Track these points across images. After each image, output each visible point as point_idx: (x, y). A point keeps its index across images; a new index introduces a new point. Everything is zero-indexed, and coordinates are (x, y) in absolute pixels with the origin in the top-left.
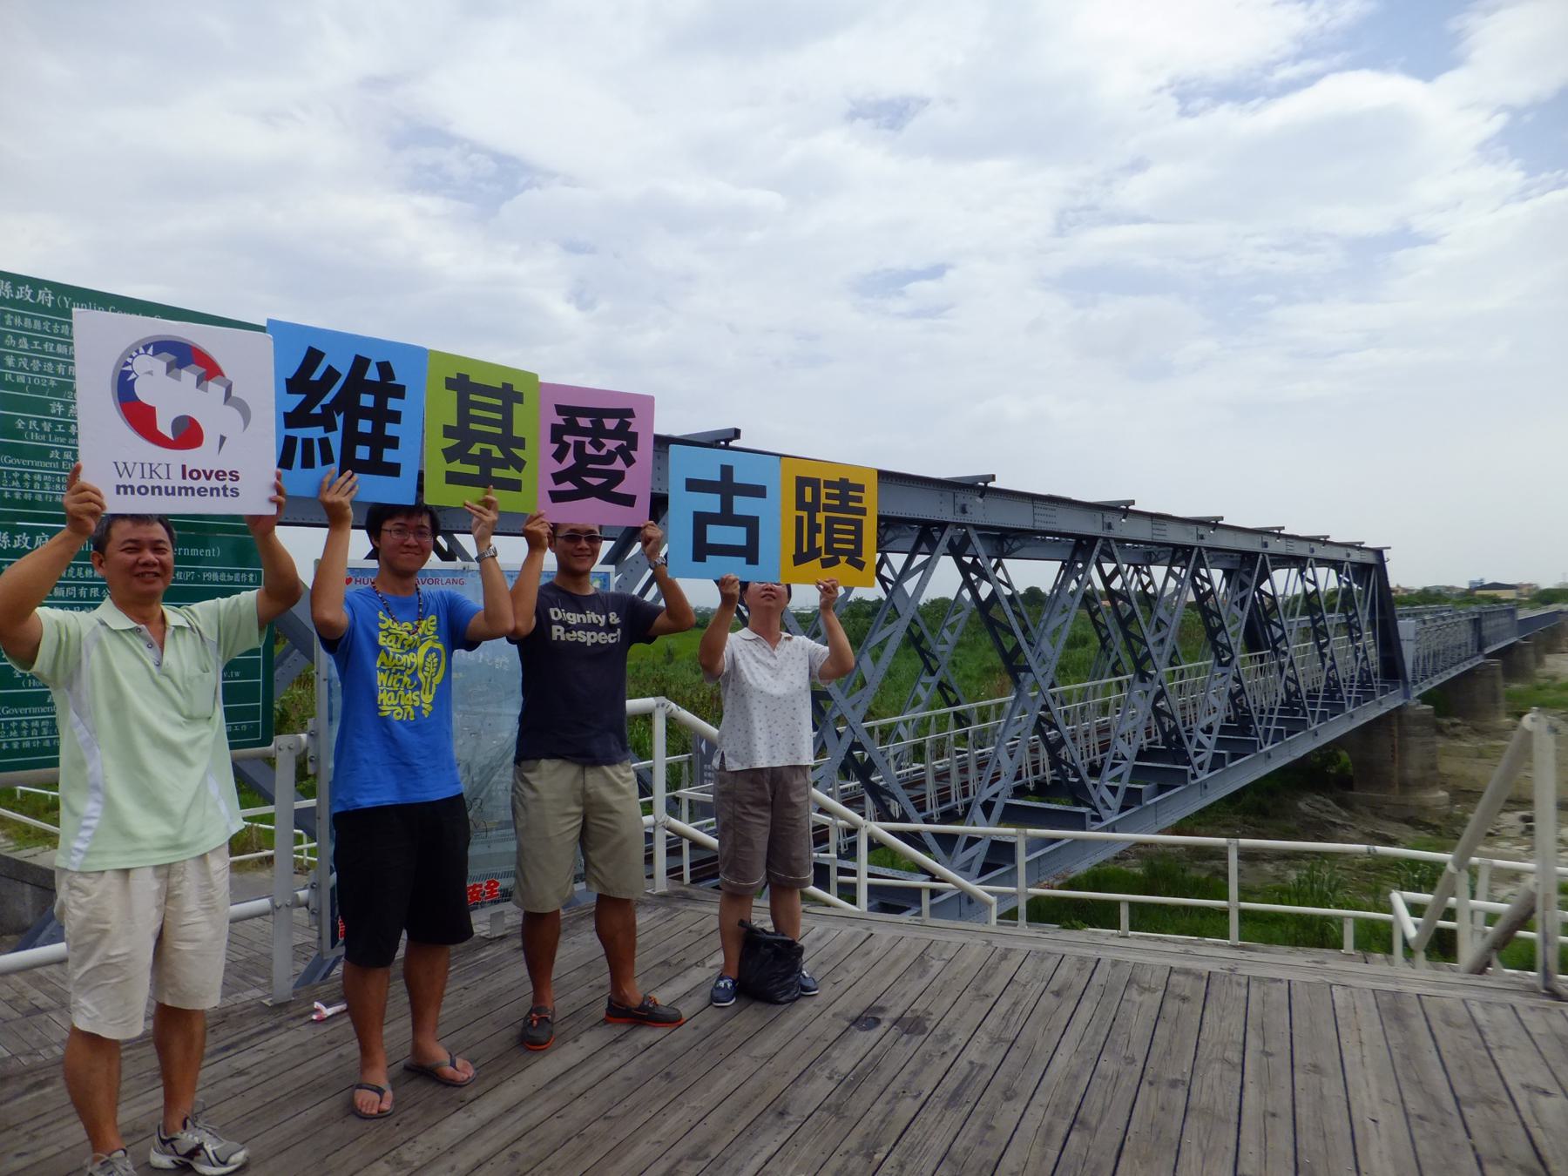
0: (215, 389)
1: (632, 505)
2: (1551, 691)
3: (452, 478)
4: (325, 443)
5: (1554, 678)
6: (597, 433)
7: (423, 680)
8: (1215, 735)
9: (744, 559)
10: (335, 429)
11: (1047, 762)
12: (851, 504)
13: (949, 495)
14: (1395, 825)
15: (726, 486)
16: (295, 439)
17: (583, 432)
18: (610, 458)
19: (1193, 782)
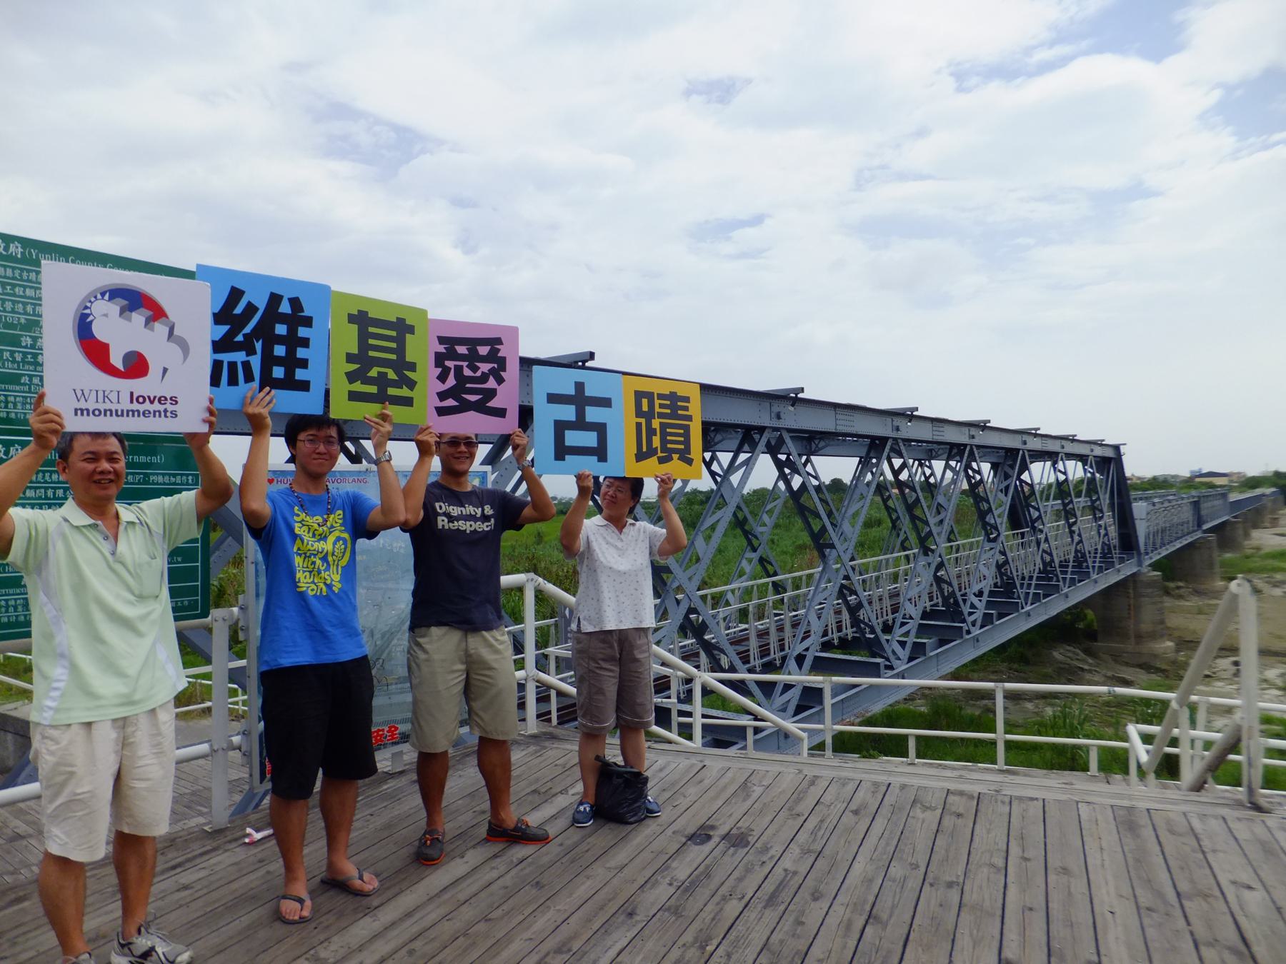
0: (160, 328)
4: (246, 365)
5: (1258, 549)
6: (473, 358)
8: (985, 598)
9: (596, 458)
10: (255, 353)
11: (848, 622)
14: (1131, 670)
15: (580, 399)
18: (484, 379)
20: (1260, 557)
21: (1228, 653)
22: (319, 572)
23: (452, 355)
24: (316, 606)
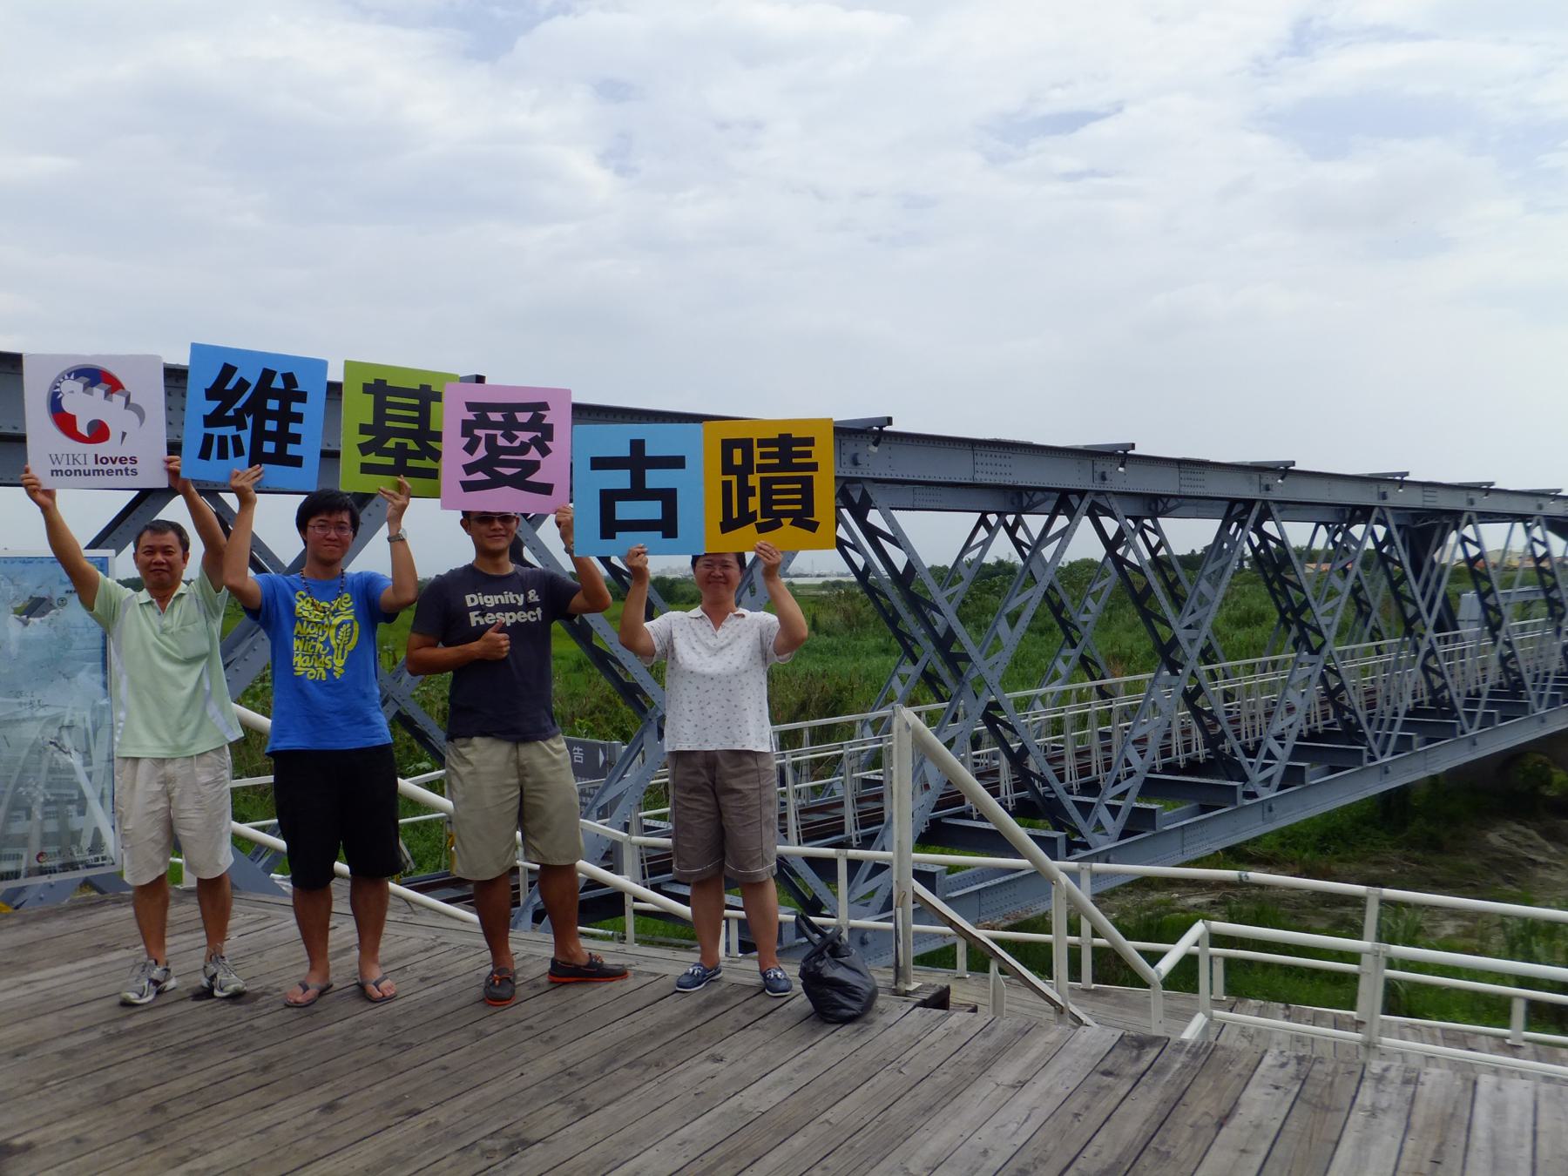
0: (118, 399)
3: (367, 469)
4: (237, 439)
6: (510, 426)
7: (335, 647)
8: (1291, 741)
9: (660, 533)
10: (245, 427)
12: (795, 461)
13: (1255, 476)
15: (638, 460)
16: (213, 436)
17: (496, 425)
18: (524, 448)
19: (1248, 802)
22: (319, 656)
23: (483, 422)
24: (316, 694)
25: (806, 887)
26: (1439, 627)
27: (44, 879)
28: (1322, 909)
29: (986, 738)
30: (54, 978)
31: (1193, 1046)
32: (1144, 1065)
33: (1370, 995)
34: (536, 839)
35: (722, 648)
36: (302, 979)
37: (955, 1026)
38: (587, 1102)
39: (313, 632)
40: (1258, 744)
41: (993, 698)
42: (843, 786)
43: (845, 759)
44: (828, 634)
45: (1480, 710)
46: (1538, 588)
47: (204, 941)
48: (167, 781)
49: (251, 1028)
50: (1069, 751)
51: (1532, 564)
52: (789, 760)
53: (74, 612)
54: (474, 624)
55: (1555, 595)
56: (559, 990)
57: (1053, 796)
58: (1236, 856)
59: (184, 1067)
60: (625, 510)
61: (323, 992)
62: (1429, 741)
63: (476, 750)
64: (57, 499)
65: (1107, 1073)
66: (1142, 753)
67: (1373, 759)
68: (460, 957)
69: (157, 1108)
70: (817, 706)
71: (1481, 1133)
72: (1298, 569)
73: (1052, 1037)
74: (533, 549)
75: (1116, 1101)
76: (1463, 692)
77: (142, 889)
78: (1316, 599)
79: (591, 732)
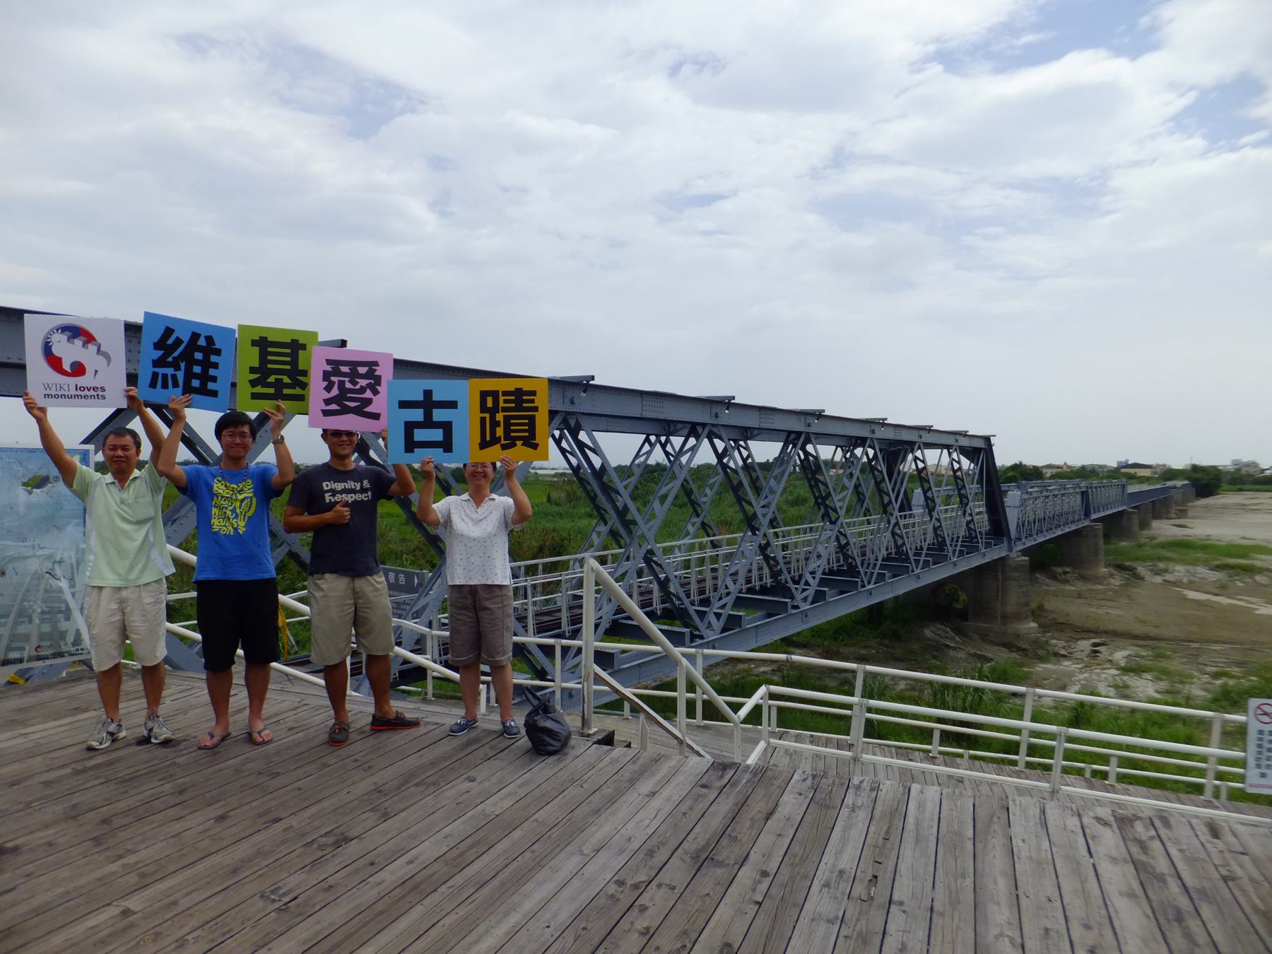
0: (92, 348)
1: (536, 449)
2: (1149, 548)
4: (174, 377)
5: (1152, 538)
6: (354, 376)
7: (239, 513)
8: (819, 575)
10: (180, 370)
12: (524, 405)
13: (802, 418)
14: (996, 648)
15: (428, 403)
17: (345, 375)
18: (363, 390)
19: (794, 611)
20: (1152, 546)
21: (1093, 635)
23: (336, 372)
25: (536, 660)
26: (901, 509)
27: (40, 663)
28: (835, 675)
29: (646, 571)
30: (41, 731)
31: (754, 768)
32: (725, 780)
33: (858, 727)
34: (364, 638)
35: (481, 520)
36: (211, 730)
37: (616, 757)
38: (388, 810)
39: (225, 504)
40: (800, 576)
41: (650, 547)
42: (562, 599)
43: (563, 583)
44: (557, 504)
45: (922, 558)
46: (954, 487)
47: (145, 705)
48: (122, 602)
49: (175, 764)
50: (693, 580)
51: (951, 473)
52: (529, 583)
53: (61, 487)
54: (328, 501)
55: (963, 492)
56: (376, 735)
57: (683, 606)
58: (788, 644)
59: (126, 792)
60: (420, 435)
61: (223, 739)
62: (894, 576)
63: (327, 582)
64: (48, 414)
65: (704, 786)
66: (735, 582)
67: (863, 586)
68: (316, 713)
69: (105, 821)
70: (549, 549)
71: (911, 820)
72: (825, 473)
73: (673, 763)
74: (375, 451)
75: (708, 804)
76: (913, 548)
77: (104, 673)
78: (834, 491)
79: (413, 563)
